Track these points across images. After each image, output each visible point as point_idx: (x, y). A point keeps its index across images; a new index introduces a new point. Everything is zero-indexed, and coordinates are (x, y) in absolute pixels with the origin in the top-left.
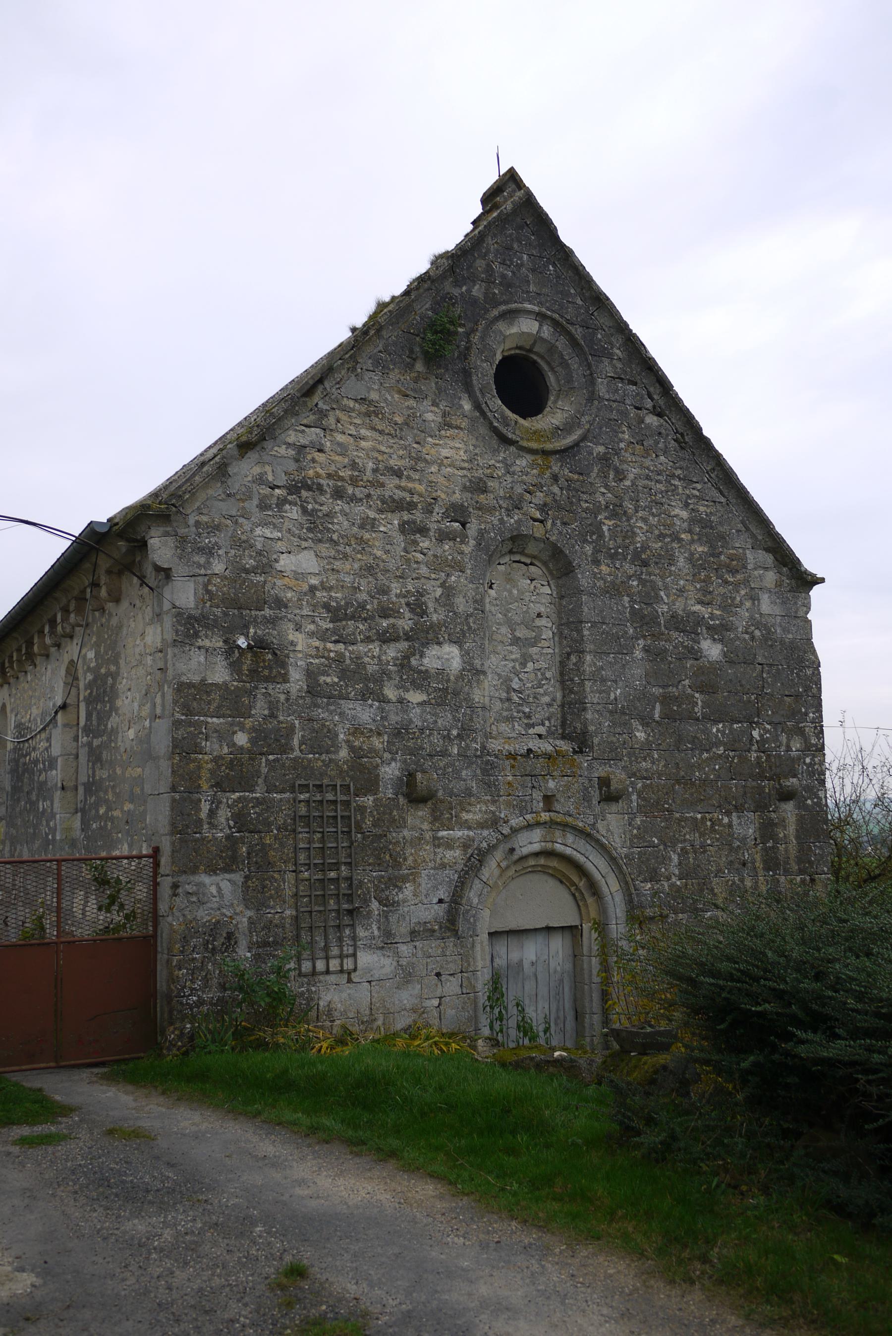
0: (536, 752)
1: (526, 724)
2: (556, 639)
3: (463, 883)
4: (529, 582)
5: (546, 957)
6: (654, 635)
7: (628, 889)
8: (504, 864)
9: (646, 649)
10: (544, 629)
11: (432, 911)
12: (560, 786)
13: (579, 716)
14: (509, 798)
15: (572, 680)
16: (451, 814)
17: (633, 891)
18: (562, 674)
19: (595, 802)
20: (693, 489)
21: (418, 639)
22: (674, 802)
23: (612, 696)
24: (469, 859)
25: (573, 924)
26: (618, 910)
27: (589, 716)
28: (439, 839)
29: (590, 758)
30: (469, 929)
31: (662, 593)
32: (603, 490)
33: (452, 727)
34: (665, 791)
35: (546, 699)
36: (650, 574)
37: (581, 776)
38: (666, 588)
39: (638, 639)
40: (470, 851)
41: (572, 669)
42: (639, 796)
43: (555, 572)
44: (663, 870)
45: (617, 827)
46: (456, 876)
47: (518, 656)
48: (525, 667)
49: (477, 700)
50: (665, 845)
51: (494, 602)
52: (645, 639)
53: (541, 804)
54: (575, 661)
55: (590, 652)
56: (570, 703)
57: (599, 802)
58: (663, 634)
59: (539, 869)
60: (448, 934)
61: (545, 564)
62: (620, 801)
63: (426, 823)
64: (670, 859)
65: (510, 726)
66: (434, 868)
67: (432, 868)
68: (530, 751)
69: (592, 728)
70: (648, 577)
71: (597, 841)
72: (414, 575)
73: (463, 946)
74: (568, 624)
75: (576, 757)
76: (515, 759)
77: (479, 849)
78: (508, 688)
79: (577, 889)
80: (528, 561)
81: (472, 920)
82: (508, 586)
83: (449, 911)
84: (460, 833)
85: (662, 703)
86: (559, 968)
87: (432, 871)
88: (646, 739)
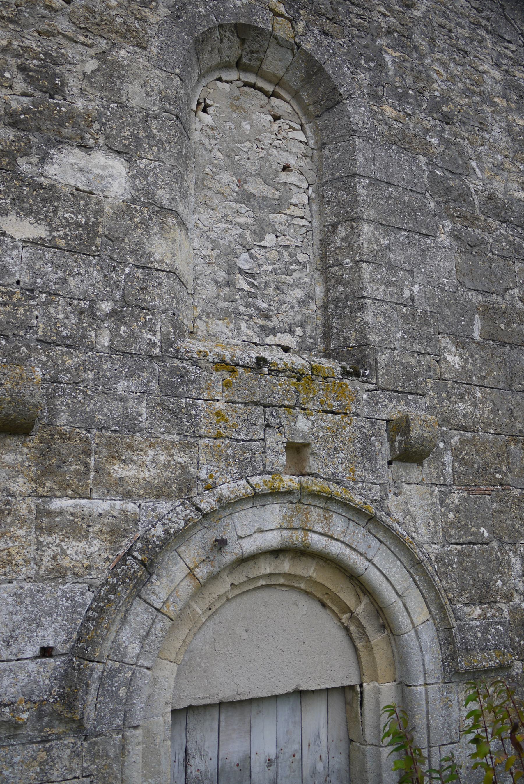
0: (274, 364)
1: (261, 327)
2: (315, 206)
3: (101, 611)
4: (271, 118)
5: (297, 747)
6: (465, 218)
7: (445, 618)
8: (202, 572)
9: (456, 236)
10: (295, 189)
11: (22, 676)
12: (320, 428)
13: (352, 319)
14: (218, 442)
15: (340, 264)
16: (86, 464)
17: (454, 623)
18: (324, 258)
19: (382, 461)
20: (506, 48)
21: (39, 129)
22: (509, 470)
23: (407, 294)
24: (123, 559)
25: (347, 683)
26: (427, 658)
27: (369, 318)
28: (50, 514)
29: (372, 387)
30: (113, 713)
31: (474, 164)
32: (382, 9)
33: (101, 296)
34: (495, 451)
35: (299, 293)
36: (456, 135)
37: (358, 415)
38: (478, 159)
39: (442, 218)
40: (126, 543)
41: (340, 248)
42: (455, 457)
43: (311, 108)
44: (499, 583)
45: (422, 507)
46: (90, 596)
47: (250, 221)
48: (262, 239)
49: (158, 257)
50: (500, 540)
51: (210, 132)
52: (452, 221)
53: (283, 459)
54: (344, 234)
55: (369, 221)
56: (337, 301)
57: (390, 463)
58: (478, 219)
59: (282, 581)
60: (59, 729)
61: (296, 95)
62: (426, 463)
63: (21, 480)
64: (509, 563)
65: (232, 326)
66: (37, 579)
67: (28, 579)
68: (261, 361)
69: (374, 338)
70: (452, 138)
71: (388, 530)
72: (43, 26)
73: (96, 755)
74: (332, 181)
75: (347, 382)
76: (232, 372)
77: (145, 539)
78: (230, 266)
79: (353, 617)
80: (270, 88)
81: (122, 692)
82: (234, 115)
83: (65, 675)
84: (105, 506)
85: (483, 317)
86: (320, 767)
87: (28, 586)
88: (463, 367)
